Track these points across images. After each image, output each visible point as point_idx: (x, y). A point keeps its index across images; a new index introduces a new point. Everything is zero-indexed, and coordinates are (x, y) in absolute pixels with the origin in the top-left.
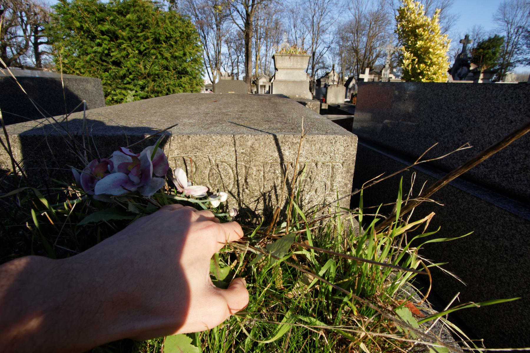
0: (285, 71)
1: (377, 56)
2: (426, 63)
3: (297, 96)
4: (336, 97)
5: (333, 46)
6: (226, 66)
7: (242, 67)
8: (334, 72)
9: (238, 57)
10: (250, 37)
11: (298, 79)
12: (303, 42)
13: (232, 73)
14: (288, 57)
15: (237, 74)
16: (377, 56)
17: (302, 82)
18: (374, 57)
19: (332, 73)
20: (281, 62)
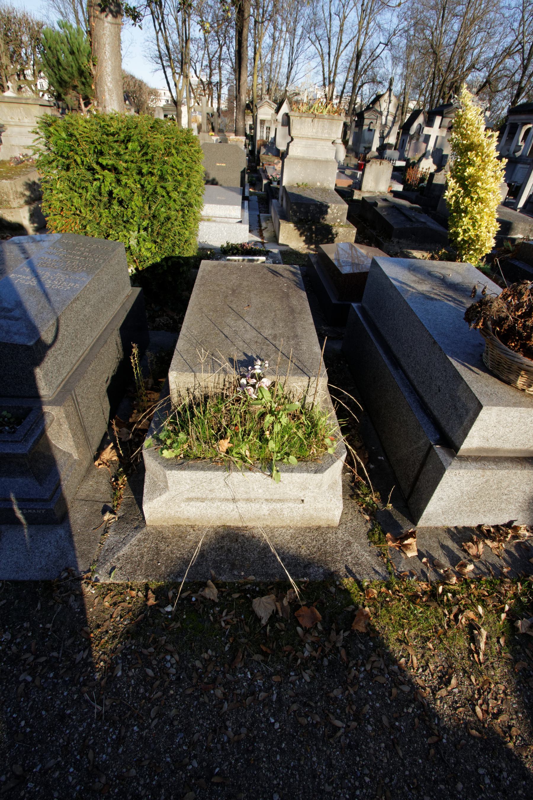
0: (304, 142)
1: (472, 66)
2: (472, 199)
3: (318, 184)
4: (377, 181)
5: (395, 40)
6: (198, 65)
7: (227, 67)
8: (390, 96)
9: (221, 47)
10: (246, 15)
11: (321, 157)
12: (342, 26)
13: (210, 83)
14: (310, 120)
15: (219, 84)
16: (472, 66)
17: (327, 162)
18: (467, 65)
19: (386, 96)
20: (298, 127)
